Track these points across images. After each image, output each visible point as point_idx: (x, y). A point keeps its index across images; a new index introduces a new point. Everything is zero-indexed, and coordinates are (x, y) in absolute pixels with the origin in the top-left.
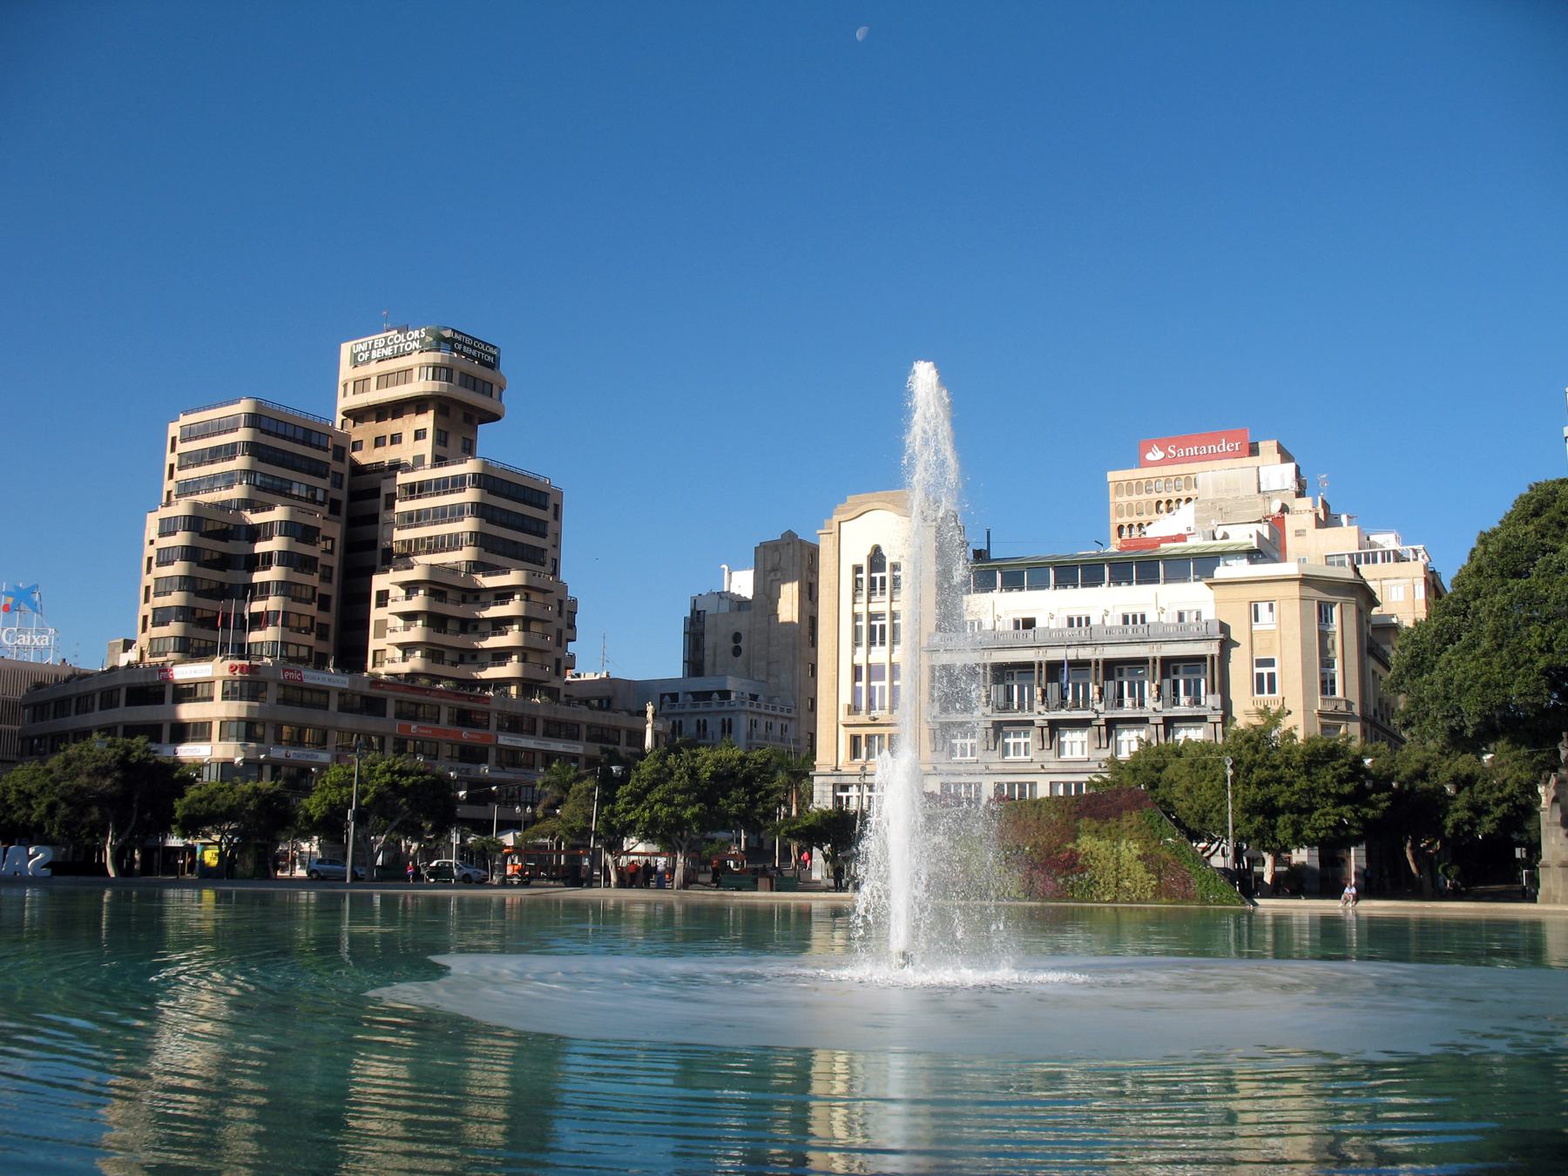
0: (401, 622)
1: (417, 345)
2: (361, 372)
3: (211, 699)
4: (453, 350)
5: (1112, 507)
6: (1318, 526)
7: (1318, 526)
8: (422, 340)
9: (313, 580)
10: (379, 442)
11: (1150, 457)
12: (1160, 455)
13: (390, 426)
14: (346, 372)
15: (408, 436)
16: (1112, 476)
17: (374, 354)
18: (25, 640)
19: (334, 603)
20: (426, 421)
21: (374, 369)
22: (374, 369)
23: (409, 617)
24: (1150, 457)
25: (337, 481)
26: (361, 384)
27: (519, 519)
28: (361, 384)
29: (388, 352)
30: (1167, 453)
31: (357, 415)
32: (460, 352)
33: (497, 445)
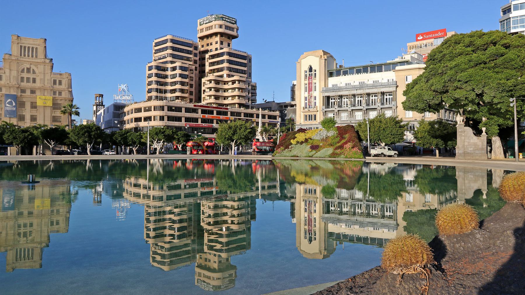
0: (208, 98)
1: (214, 19)
2: (202, 27)
4: (223, 20)
5: (194, 88)
6: (103, 95)
7: (103, 95)
8: (215, 18)
9: (186, 80)
10: (208, 45)
11: (419, 38)
12: (422, 38)
13: (210, 40)
14: (199, 28)
15: (214, 43)
16: (409, 44)
17: (205, 22)
18: (124, 98)
19: (194, 86)
20: (218, 39)
21: (204, 26)
22: (204, 26)
23: (210, 96)
24: (419, 38)
25: (195, 55)
26: (202, 30)
27: (241, 63)
28: (202, 30)
29: (207, 21)
30: (423, 37)
31: (202, 38)
32: (225, 20)
33: (236, 46)
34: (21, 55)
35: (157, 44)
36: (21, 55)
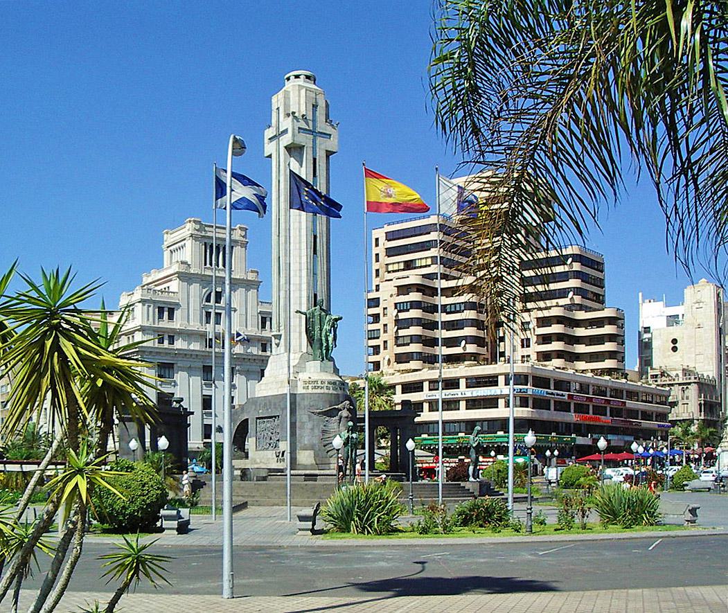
3: (438, 389)
34: (205, 264)
35: (391, 236)
36: (205, 264)
